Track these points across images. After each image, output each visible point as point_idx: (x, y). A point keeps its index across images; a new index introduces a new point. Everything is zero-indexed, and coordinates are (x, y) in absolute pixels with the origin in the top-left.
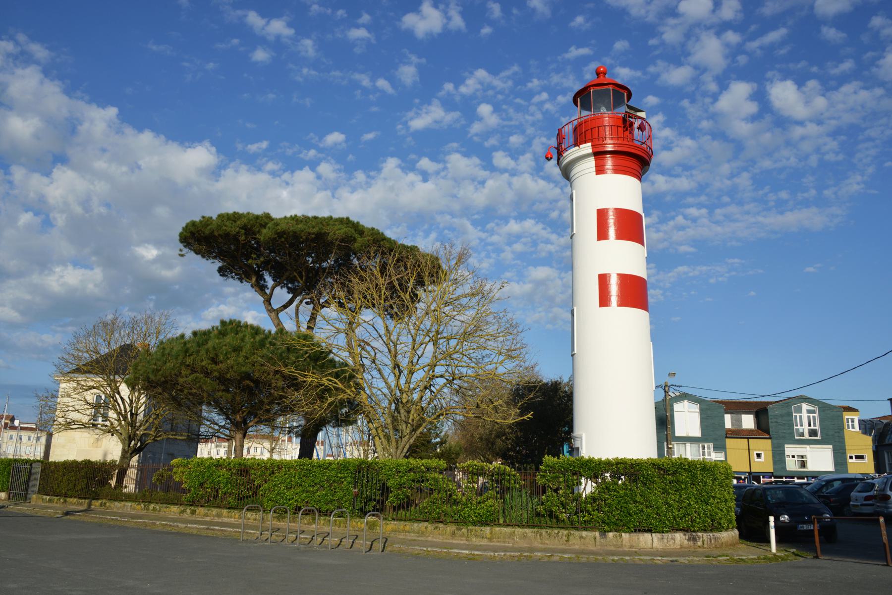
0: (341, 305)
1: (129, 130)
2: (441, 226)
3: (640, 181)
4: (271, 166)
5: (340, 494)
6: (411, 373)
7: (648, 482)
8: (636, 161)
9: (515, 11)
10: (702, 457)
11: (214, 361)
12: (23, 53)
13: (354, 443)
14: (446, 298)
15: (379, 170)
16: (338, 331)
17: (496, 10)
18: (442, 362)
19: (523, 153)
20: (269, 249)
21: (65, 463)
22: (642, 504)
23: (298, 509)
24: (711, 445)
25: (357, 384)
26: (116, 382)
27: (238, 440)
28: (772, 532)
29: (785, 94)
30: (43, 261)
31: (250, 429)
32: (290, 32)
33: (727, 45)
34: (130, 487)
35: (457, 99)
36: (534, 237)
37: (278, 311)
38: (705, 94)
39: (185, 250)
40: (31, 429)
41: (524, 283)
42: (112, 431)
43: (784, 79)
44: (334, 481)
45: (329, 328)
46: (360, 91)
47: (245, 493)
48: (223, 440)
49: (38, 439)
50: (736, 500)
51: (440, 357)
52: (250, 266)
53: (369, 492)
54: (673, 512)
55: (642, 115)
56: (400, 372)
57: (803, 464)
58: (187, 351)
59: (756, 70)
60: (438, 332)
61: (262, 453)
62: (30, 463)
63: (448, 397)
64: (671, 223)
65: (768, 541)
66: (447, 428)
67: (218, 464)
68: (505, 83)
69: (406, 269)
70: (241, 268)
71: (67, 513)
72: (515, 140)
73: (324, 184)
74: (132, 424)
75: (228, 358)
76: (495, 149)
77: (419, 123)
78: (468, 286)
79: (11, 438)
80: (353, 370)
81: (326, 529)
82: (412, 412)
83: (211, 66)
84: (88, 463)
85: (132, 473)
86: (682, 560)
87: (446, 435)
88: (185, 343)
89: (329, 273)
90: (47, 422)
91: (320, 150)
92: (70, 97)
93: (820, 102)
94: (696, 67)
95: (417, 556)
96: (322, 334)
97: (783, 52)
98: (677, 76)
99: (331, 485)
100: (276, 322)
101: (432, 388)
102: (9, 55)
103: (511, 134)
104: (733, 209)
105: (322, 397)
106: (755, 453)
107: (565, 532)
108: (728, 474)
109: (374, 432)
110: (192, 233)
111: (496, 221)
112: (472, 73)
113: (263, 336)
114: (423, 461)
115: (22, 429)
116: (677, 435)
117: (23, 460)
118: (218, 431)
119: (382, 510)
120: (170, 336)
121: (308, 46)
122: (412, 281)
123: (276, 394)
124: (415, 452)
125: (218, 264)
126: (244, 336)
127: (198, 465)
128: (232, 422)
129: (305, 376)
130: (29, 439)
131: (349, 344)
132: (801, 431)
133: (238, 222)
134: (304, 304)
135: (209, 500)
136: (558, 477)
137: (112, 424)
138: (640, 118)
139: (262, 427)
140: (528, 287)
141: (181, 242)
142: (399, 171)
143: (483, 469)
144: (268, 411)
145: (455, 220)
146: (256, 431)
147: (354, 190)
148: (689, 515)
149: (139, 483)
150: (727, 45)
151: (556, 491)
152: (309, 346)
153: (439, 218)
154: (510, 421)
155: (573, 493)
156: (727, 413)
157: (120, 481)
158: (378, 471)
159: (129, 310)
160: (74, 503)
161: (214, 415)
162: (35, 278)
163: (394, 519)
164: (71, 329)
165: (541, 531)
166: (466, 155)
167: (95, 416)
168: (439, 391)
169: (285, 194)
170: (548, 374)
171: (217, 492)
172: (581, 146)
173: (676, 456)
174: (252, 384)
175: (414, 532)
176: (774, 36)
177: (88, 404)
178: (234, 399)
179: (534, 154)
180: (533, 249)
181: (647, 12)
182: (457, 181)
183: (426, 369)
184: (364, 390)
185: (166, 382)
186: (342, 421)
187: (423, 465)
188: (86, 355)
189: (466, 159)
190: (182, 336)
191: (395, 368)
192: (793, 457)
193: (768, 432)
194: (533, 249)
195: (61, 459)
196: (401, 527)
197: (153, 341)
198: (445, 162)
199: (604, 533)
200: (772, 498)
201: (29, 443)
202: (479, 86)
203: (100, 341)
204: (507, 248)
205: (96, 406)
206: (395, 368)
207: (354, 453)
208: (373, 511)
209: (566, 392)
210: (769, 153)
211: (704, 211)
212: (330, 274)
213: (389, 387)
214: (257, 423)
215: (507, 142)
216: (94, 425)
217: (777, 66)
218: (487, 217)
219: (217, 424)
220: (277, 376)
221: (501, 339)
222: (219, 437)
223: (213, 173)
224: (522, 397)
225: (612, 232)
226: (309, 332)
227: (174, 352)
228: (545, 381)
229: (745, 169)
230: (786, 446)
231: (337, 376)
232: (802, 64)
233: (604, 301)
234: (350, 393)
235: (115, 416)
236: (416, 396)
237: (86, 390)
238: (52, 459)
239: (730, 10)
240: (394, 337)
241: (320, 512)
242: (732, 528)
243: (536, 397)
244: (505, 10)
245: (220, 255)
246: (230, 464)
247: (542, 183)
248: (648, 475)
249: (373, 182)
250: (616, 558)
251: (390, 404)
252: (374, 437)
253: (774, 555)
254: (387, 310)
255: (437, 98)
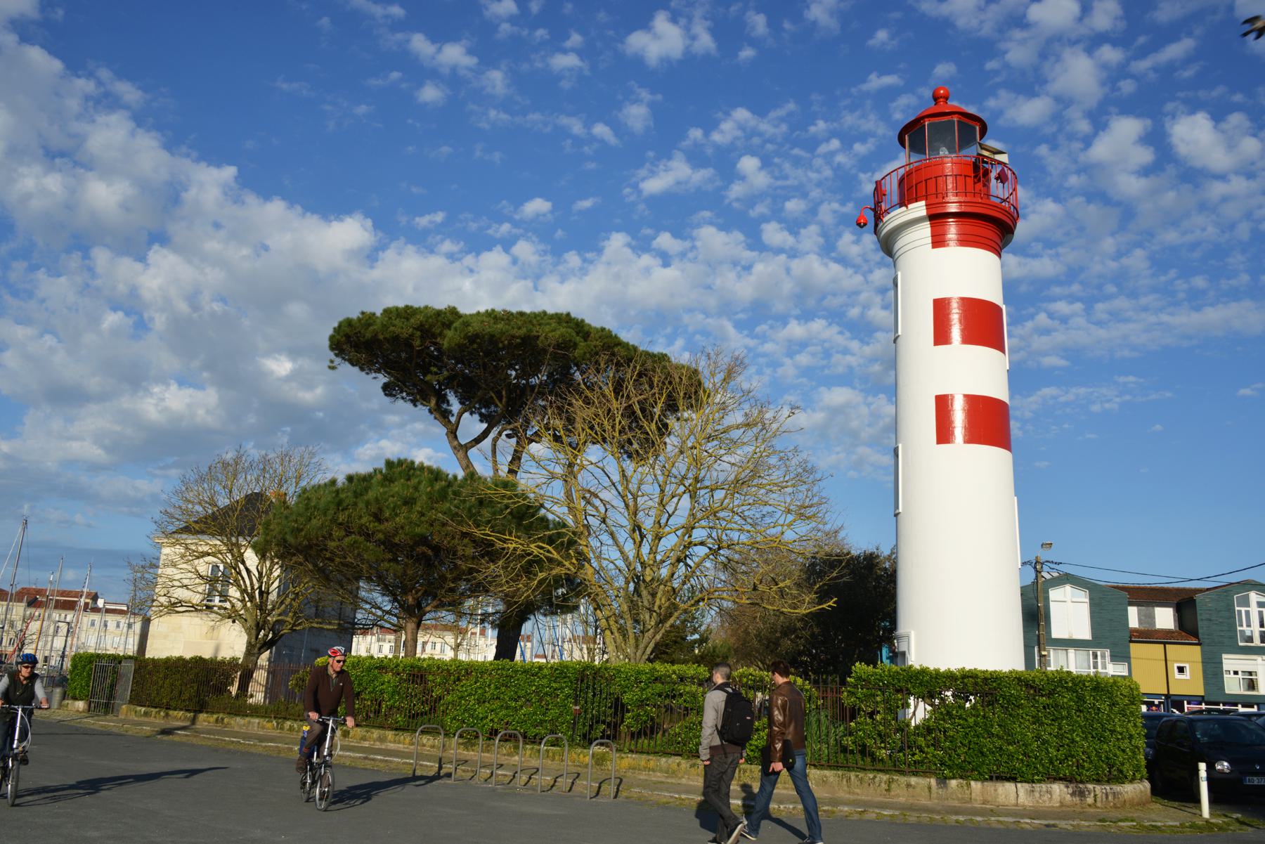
0: (557, 439)
1: (251, 199)
2: (691, 329)
3: (1000, 256)
4: (448, 246)
5: (554, 712)
6: (658, 538)
7: (1011, 705)
8: (993, 228)
9: (787, 25)
10: (1092, 670)
11: (377, 517)
12: (107, 95)
13: (574, 639)
14: (709, 430)
15: (600, 251)
16: (553, 476)
17: (759, 23)
18: (703, 523)
19: (805, 225)
20: (455, 358)
21: (168, 660)
22: (1000, 738)
23: (494, 733)
24: (1108, 653)
25: (580, 554)
26: (239, 546)
27: (409, 631)
28: (1204, 787)
29: (1194, 134)
30: (135, 378)
31: (427, 616)
32: (471, 61)
33: (1104, 66)
34: (257, 695)
35: (709, 151)
36: (826, 345)
37: (466, 447)
38: (1071, 137)
39: (338, 360)
40: (121, 612)
41: (814, 410)
42: (233, 616)
43: (1192, 111)
44: (546, 694)
45: (539, 471)
46: (569, 141)
47: (420, 708)
48: (389, 631)
49: (130, 626)
50: (1146, 736)
51: (699, 515)
52: (429, 384)
53: (597, 710)
54: (1048, 752)
55: (1003, 158)
56: (642, 536)
57: (1252, 685)
58: (340, 503)
59: (1152, 101)
60: (697, 480)
61: (442, 651)
62: (117, 660)
63: (711, 574)
64: (1029, 324)
65: (1198, 801)
66: (709, 619)
67: (382, 666)
68: (776, 126)
69: (652, 387)
70: (415, 385)
71: (167, 732)
72: (794, 206)
73: (521, 270)
74: (261, 607)
75: (396, 515)
76: (765, 219)
77: (654, 185)
78: (742, 413)
79: (93, 624)
80: (574, 533)
81: (535, 763)
82: (659, 595)
83: (362, 109)
84: (198, 661)
85: (260, 676)
86: (1063, 824)
87: (709, 630)
88: (337, 492)
89: (539, 393)
90: (143, 602)
91: (516, 224)
92: (172, 154)
93: (1250, 146)
94: (1058, 99)
95: (665, 806)
96: (529, 480)
97: (1188, 73)
98: (1030, 112)
99: (541, 700)
100: (464, 462)
101: (688, 561)
102: (87, 98)
103: (788, 199)
104: (1122, 303)
105: (528, 570)
106: (1176, 665)
107: (885, 777)
108: (1134, 697)
109: (603, 623)
110: (347, 336)
111: (770, 322)
112: (727, 114)
113: (443, 483)
114: (675, 667)
115: (108, 611)
116: (1054, 635)
117: (109, 656)
118: (382, 618)
119: (614, 737)
120: (315, 482)
121: (497, 79)
122: (660, 405)
123: (464, 566)
124: (665, 653)
125: (383, 379)
126: (419, 483)
127: (354, 667)
128: (401, 606)
129: (505, 541)
130: (118, 626)
131: (569, 495)
132: (1248, 633)
133: (412, 320)
134: (503, 436)
135: (368, 717)
136: (874, 696)
137: (233, 606)
138: (1000, 163)
139: (444, 613)
140: (819, 417)
141: (332, 349)
142: (628, 251)
143: (762, 680)
144: (452, 590)
145: (709, 320)
146: (435, 619)
147: (563, 279)
148: (1073, 756)
149: (270, 690)
150: (1104, 66)
151: (871, 715)
152: (510, 498)
153: (686, 318)
154: (803, 610)
155: (896, 719)
156: (1131, 604)
157: (243, 687)
158: (610, 681)
159: (254, 447)
160: (179, 717)
161: (375, 595)
162: (126, 402)
163: (631, 751)
164: (175, 473)
165: (848, 774)
166: (724, 228)
167: (209, 595)
168: (698, 565)
169: (467, 284)
170: (858, 541)
171: (380, 705)
172: (910, 206)
173: (1052, 668)
174: (430, 552)
175: (661, 771)
176: (1175, 51)
177: (201, 577)
178: (405, 574)
179: (822, 224)
180: (825, 362)
181: (982, 22)
182: (713, 265)
183: (679, 533)
184: (589, 561)
185: (310, 547)
186: (558, 606)
187: (674, 672)
188: (199, 508)
189: (723, 234)
190: (333, 482)
191: (634, 531)
192: (1236, 673)
193: (1196, 635)
194: (825, 362)
195: (163, 655)
196: (643, 763)
197: (291, 490)
198: (693, 239)
199: (943, 780)
200: (1203, 735)
201: (118, 632)
202: (739, 133)
203: (218, 488)
204: (788, 361)
205: (212, 581)
206: (634, 531)
207: (577, 654)
208: (602, 738)
209: (885, 569)
210: (1173, 221)
211: (1078, 306)
212: (541, 395)
213: (626, 559)
214: (437, 607)
215: (782, 209)
216: (208, 607)
217: (1181, 94)
218: (757, 315)
219: (380, 608)
220: (466, 541)
221: (789, 490)
222: (382, 627)
223: (368, 257)
224: (821, 575)
225: (956, 332)
226: (511, 477)
227: (322, 505)
228: (854, 553)
229: (1140, 245)
230: (1224, 656)
231: (551, 541)
232: (1219, 91)
233: (944, 435)
234: (569, 566)
235: (238, 595)
236: (664, 572)
237: (198, 558)
238: (148, 655)
239: (1105, 16)
240: (633, 487)
241: (525, 737)
242: (1141, 779)
243: (842, 576)
244: (773, 24)
245: (386, 367)
246: (397, 665)
247: (835, 268)
248: (1012, 695)
249: (591, 267)
250: (961, 818)
251: (627, 583)
252: (603, 631)
253: (1207, 821)
254: (623, 447)
255: (679, 149)
